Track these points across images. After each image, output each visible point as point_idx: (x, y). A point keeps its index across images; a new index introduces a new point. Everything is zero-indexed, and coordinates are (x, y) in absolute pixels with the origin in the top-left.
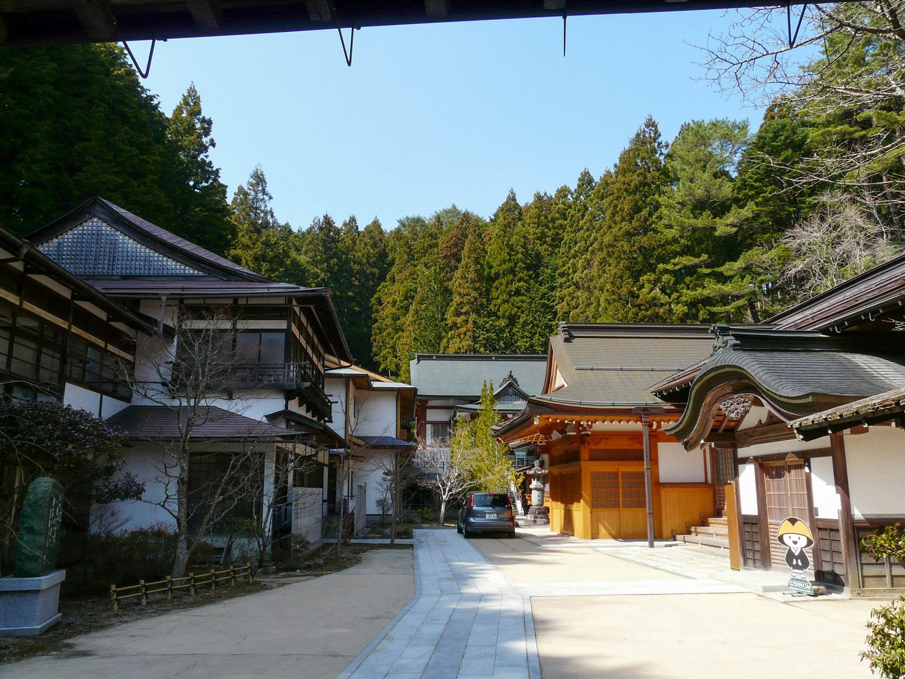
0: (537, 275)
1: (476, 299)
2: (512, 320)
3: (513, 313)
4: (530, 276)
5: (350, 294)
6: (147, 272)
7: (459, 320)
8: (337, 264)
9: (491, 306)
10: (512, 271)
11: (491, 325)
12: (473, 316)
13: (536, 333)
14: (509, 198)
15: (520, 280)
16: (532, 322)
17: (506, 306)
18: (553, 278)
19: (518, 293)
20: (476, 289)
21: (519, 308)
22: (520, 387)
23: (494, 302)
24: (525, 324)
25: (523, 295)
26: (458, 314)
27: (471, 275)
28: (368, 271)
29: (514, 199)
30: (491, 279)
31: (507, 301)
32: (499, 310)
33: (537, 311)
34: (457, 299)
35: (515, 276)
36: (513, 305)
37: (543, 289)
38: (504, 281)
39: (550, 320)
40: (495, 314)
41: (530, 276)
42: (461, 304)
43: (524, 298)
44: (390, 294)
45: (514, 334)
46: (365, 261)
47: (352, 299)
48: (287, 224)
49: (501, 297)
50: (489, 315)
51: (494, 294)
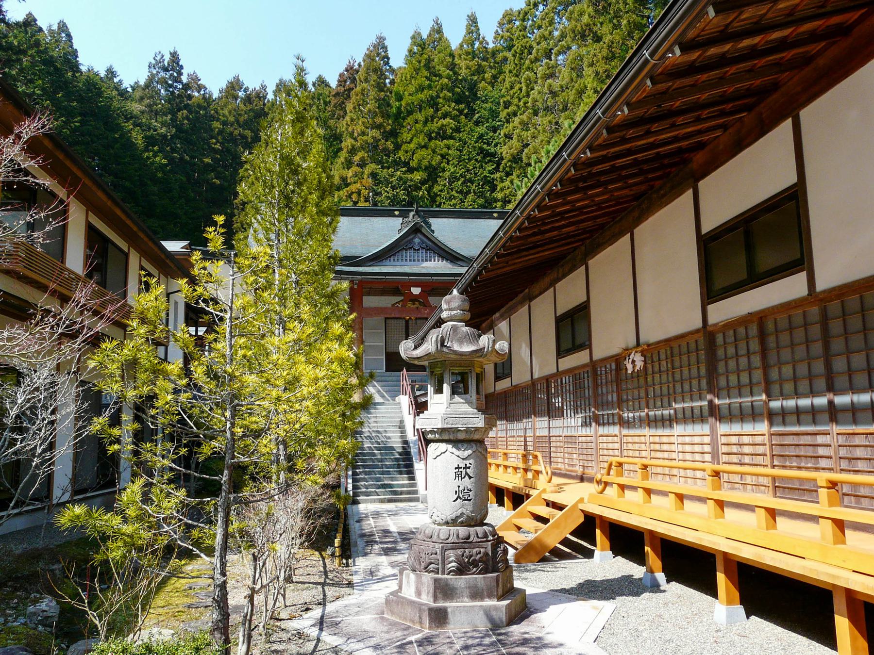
0: (472, 111)
1: (377, 140)
2: (433, 173)
3: (434, 163)
4: (461, 112)
5: (208, 160)
6: (707, 440)
7: (350, 173)
8: (187, 118)
9: (400, 154)
10: (433, 103)
11: (400, 178)
12: (372, 167)
13: (469, 192)
14: (433, 29)
15: (444, 116)
16: (461, 176)
17: (423, 152)
18: (494, 114)
19: (442, 135)
20: (378, 127)
21: (443, 156)
22: (435, 234)
23: (404, 147)
24: (453, 179)
25: (451, 137)
26: (349, 164)
27: (371, 105)
28: (236, 132)
29: (439, 31)
30: (399, 117)
31: (425, 147)
32: (411, 159)
33: (470, 159)
34: (348, 143)
35: (437, 110)
36: (434, 151)
37: (481, 129)
38: (420, 117)
39: (491, 172)
40: (406, 164)
41: (461, 112)
42: (353, 151)
43: (451, 142)
44: (264, 161)
45: (436, 195)
46: (232, 119)
47: (207, 168)
48: (63, 27)
49: (415, 140)
50: (397, 164)
51: (406, 136)
